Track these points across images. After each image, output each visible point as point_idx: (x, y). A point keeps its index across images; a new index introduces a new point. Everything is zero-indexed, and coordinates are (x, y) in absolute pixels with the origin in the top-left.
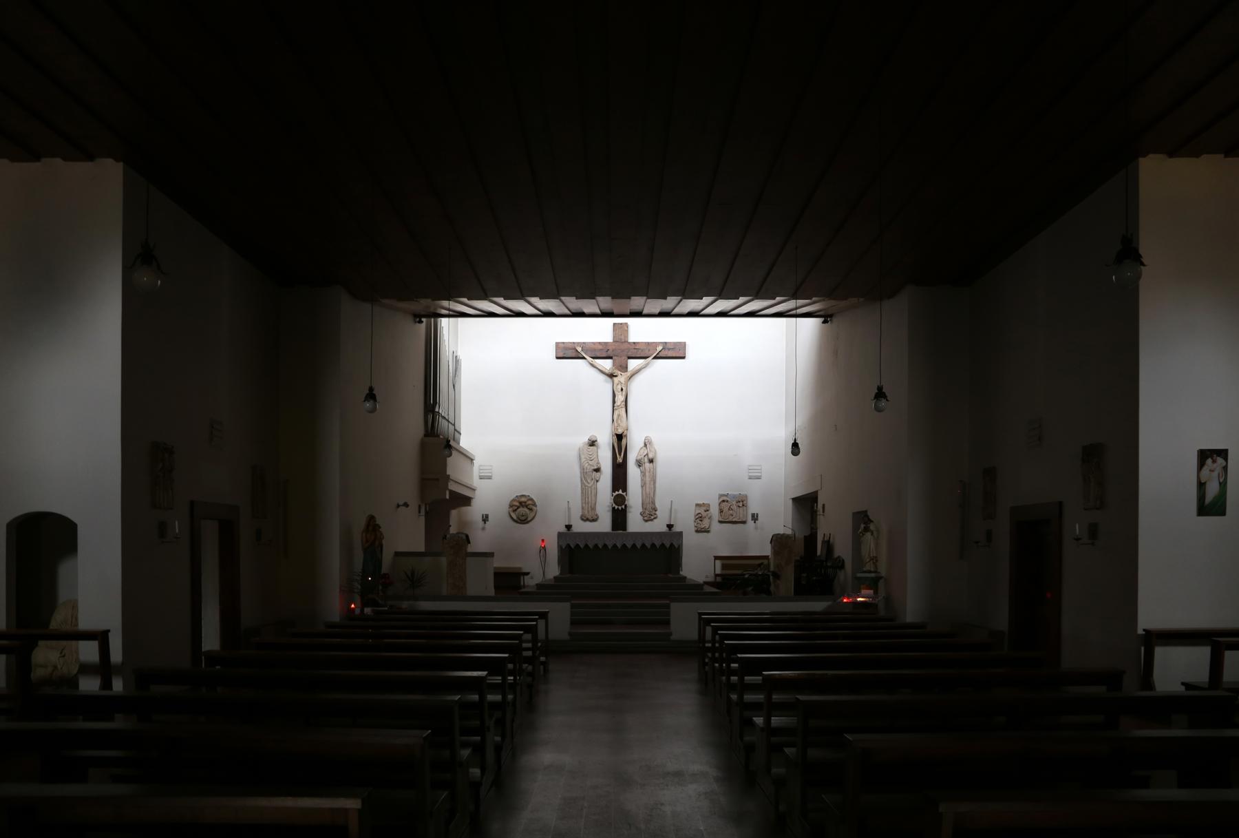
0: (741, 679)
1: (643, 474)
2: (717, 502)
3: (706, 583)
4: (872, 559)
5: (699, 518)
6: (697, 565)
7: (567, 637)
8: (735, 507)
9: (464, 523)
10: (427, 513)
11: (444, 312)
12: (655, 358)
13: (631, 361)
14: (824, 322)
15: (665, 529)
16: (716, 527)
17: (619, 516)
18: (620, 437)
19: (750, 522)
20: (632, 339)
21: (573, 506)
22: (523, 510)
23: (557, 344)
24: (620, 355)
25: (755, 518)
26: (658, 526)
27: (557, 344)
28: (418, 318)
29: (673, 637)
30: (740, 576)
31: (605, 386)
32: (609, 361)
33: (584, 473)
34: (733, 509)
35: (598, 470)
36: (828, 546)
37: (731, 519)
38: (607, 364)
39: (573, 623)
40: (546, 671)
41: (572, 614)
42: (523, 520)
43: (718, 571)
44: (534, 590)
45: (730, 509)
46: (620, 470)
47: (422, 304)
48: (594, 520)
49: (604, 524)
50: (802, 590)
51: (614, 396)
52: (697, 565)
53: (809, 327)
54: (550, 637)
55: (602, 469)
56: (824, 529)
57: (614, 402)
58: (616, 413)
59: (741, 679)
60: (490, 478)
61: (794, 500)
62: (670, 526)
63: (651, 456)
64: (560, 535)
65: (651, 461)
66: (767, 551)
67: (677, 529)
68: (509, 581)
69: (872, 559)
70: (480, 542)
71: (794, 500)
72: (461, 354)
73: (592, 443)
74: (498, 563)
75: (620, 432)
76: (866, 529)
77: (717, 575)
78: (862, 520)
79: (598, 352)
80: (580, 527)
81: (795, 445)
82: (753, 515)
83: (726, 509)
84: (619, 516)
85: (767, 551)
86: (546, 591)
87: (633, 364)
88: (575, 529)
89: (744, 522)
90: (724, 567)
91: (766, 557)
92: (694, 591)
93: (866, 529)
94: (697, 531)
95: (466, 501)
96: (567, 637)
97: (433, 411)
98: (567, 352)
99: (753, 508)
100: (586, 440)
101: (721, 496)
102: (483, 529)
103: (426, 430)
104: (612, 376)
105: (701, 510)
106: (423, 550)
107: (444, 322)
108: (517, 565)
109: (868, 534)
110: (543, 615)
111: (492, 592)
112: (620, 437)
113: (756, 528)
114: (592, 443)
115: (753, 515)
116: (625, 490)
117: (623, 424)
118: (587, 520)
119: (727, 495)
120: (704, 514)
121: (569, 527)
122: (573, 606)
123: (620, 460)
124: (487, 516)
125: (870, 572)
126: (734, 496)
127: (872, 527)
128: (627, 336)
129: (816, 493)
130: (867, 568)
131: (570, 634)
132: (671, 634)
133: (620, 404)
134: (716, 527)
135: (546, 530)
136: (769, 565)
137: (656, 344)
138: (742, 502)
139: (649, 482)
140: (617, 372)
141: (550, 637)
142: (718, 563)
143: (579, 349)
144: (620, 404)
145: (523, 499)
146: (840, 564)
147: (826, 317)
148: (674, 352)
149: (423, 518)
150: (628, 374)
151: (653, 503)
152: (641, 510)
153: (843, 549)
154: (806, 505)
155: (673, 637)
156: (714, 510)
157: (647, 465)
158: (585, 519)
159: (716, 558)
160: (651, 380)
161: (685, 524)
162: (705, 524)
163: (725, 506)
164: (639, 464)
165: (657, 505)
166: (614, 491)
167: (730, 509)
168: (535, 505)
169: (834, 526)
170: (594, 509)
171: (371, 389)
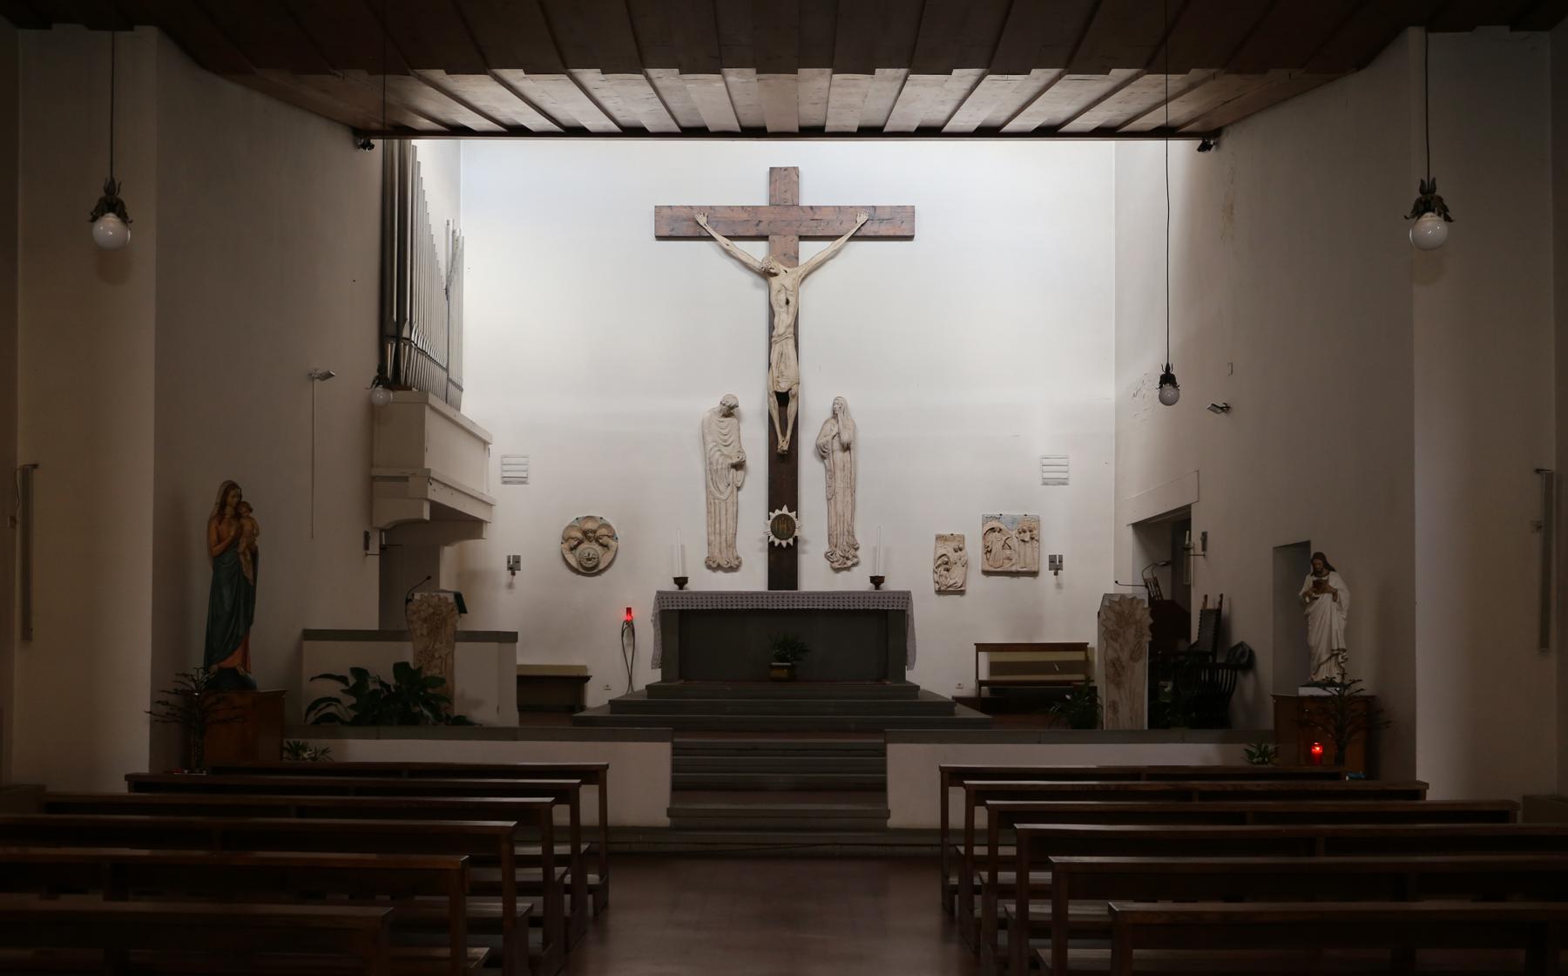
0: (1022, 877)
1: (831, 473)
2: (980, 532)
3: (958, 700)
4: (1334, 655)
5: (944, 564)
6: (942, 663)
7: (664, 820)
8: (1014, 542)
9: (470, 576)
10: (382, 548)
11: (425, 124)
12: (854, 238)
13: (804, 245)
14: (1203, 148)
15: (867, 586)
16: (977, 584)
17: (783, 563)
18: (783, 399)
19: (1046, 574)
20: (806, 200)
21: (698, 542)
22: (589, 548)
23: (658, 209)
24: (781, 229)
25: (1056, 564)
26: (856, 581)
27: (658, 209)
28: (362, 136)
29: (893, 822)
30: (1029, 691)
31: (753, 296)
32: (762, 245)
33: (711, 472)
34: (1012, 550)
35: (739, 466)
36: (1217, 620)
37: (1007, 567)
38: (757, 252)
39: (677, 787)
40: (602, 906)
41: (675, 768)
42: (590, 569)
43: (984, 676)
44: (606, 713)
45: (1006, 546)
46: (783, 467)
47: (358, 91)
48: (733, 569)
49: (752, 578)
50: (1165, 718)
51: (772, 314)
52: (942, 663)
53: (1164, 164)
54: (612, 819)
55: (748, 463)
56: (1207, 583)
57: (772, 327)
58: (776, 349)
59: (1022, 877)
60: (523, 481)
61: (1139, 527)
62: (877, 581)
63: (845, 437)
64: (661, 596)
65: (846, 448)
66: (1087, 632)
67: (890, 585)
68: (552, 697)
69: (1334, 655)
70: (501, 607)
71: (1139, 527)
72: (466, 231)
73: (729, 411)
74: (531, 656)
75: (783, 387)
76: (1320, 587)
77: (981, 684)
78: (1303, 566)
79: (740, 227)
80: (705, 582)
81: (1167, 379)
82: (1052, 559)
83: (997, 547)
84: (783, 563)
85: (1087, 632)
86: (630, 717)
87: (810, 251)
88: (692, 586)
89: (1034, 574)
90: (994, 667)
91: (1082, 647)
92: (933, 718)
93: (1320, 587)
94: (939, 592)
95: (471, 527)
96: (664, 820)
97: (398, 338)
98: (681, 227)
99: (1052, 543)
100: (715, 404)
101: (987, 519)
102: (510, 586)
103: (382, 368)
104: (767, 274)
105: (948, 549)
106: (375, 627)
107: (425, 151)
108: (576, 661)
109: (1326, 598)
110: (594, 775)
111: (512, 718)
112: (783, 399)
113: (1059, 586)
114: (729, 411)
115: (1052, 559)
116: (794, 507)
117: (790, 373)
118: (719, 567)
119: (998, 518)
120: (953, 556)
121: (681, 582)
122: (676, 750)
123: (783, 445)
124: (517, 560)
125: (1330, 683)
126: (1014, 520)
127: (1334, 580)
128: (796, 194)
129: (1186, 510)
130: (1323, 674)
131: (670, 813)
132: (887, 814)
133: (783, 333)
134: (977, 584)
135: (635, 590)
136: (1086, 665)
137: (855, 210)
138: (1029, 532)
139: (842, 490)
140: (778, 267)
141: (612, 819)
142: (983, 656)
143: (702, 220)
144: (783, 333)
145: (590, 525)
146: (1244, 660)
147: (1208, 137)
148: (889, 227)
149: (374, 562)
150: (801, 271)
151: (851, 534)
152: (826, 548)
153: (1252, 626)
154: (1166, 537)
155: (893, 822)
156: (974, 550)
157: (839, 456)
158: (714, 566)
159: (980, 647)
160: (840, 283)
161: (909, 574)
162: (955, 577)
163: (996, 541)
164: (823, 453)
165: (859, 538)
166: (771, 509)
167: (1006, 546)
168: (613, 536)
169: (1231, 578)
170: (731, 545)
171: (111, 188)
